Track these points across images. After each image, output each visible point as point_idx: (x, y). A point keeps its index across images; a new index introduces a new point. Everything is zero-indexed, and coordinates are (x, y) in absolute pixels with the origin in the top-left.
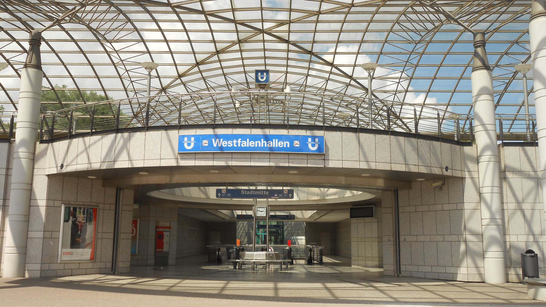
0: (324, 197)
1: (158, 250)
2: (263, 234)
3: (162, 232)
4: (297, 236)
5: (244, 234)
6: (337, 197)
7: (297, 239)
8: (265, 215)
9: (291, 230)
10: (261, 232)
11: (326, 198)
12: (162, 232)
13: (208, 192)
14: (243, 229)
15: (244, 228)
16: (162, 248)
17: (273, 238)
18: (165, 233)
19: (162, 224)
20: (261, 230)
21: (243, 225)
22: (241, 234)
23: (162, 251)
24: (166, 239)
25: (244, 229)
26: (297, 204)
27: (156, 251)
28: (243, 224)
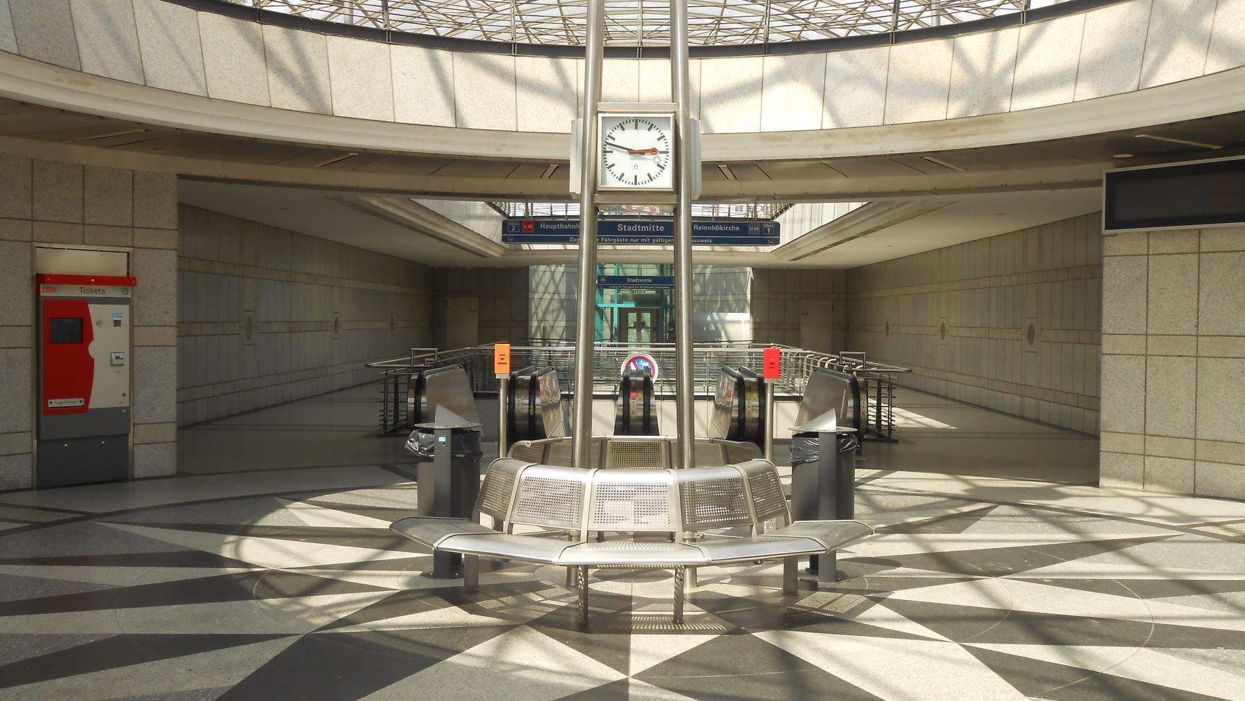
0: (993, 100)
1: (54, 403)
2: (616, 306)
4: (721, 310)
5: (555, 305)
6: (1084, 91)
7: (723, 322)
8: (665, 181)
9: (703, 293)
10: (609, 299)
11: (1006, 106)
13: (322, 79)
14: (552, 289)
15: (557, 286)
16: (86, 392)
17: (647, 317)
18: (95, 311)
20: (609, 293)
21: (553, 278)
22: (544, 304)
23: (84, 409)
25: (557, 292)
26: (818, 152)
27: (41, 410)
28: (553, 273)
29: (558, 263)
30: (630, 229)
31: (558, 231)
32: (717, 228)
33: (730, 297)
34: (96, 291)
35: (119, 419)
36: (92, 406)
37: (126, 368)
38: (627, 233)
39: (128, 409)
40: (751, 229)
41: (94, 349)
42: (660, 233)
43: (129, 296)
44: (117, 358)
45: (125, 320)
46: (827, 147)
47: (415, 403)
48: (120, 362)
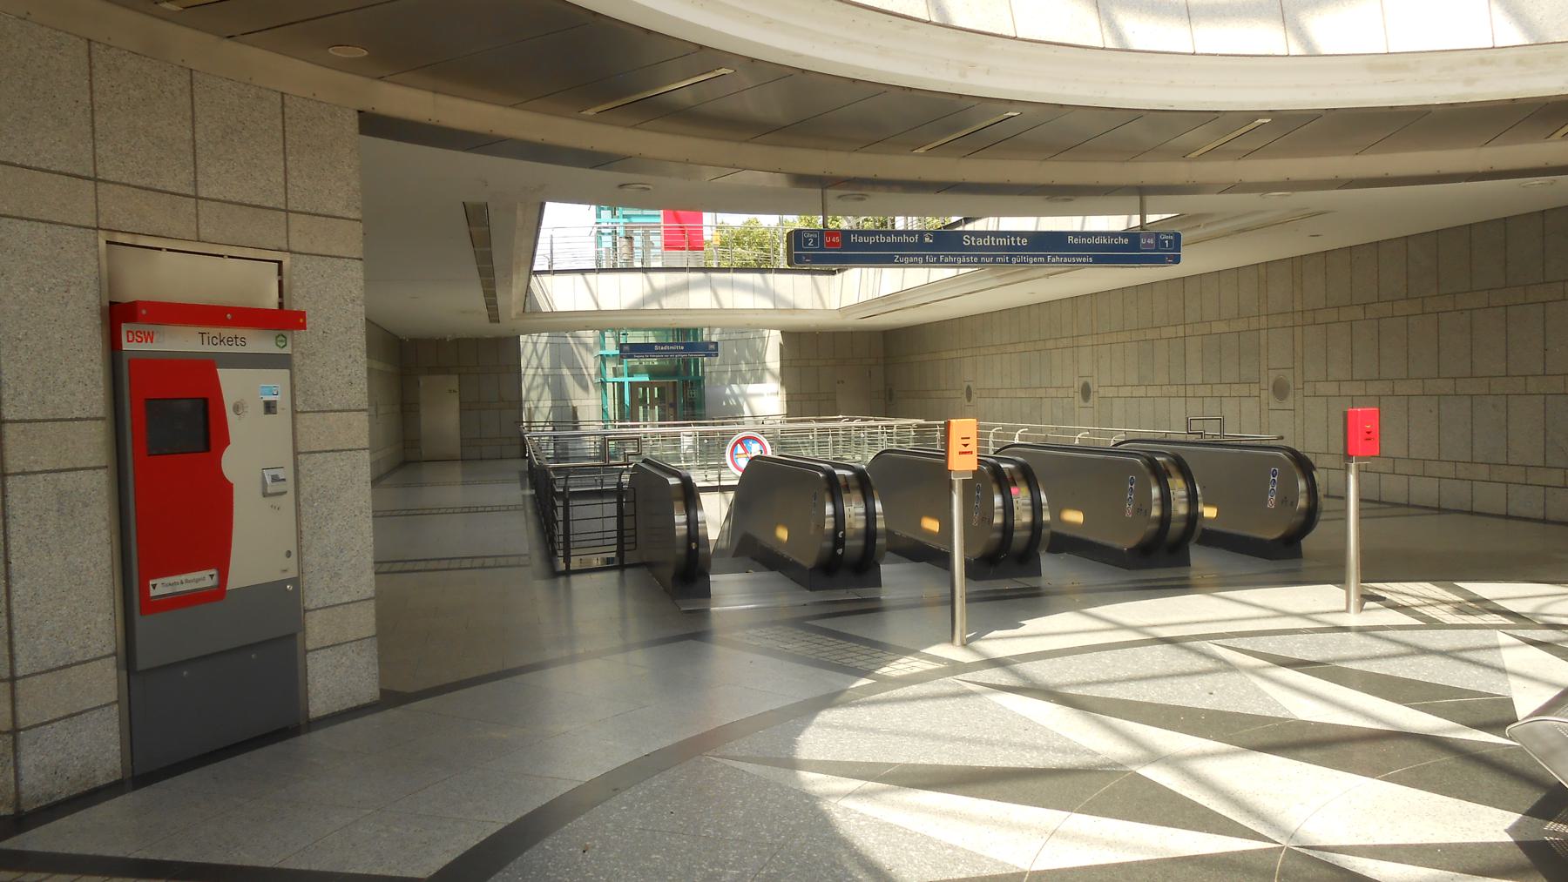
1: (161, 587)
3: (203, 371)
5: (539, 380)
7: (745, 396)
12: (203, 371)
14: (534, 362)
15: (540, 359)
16: (216, 553)
18: (232, 383)
19: (170, 275)
21: (535, 349)
24: (250, 454)
25: (540, 366)
27: (134, 603)
28: (535, 344)
29: (539, 331)
30: (980, 242)
31: (876, 246)
32: (1098, 241)
33: (744, 367)
34: (230, 341)
35: (283, 600)
36: (233, 583)
37: (289, 499)
38: (977, 248)
39: (295, 581)
40: (1143, 241)
41: (235, 464)
42: (1022, 248)
43: (287, 350)
44: (275, 479)
45: (282, 400)
46: (1469, 82)
47: (688, 523)
48: (279, 487)
